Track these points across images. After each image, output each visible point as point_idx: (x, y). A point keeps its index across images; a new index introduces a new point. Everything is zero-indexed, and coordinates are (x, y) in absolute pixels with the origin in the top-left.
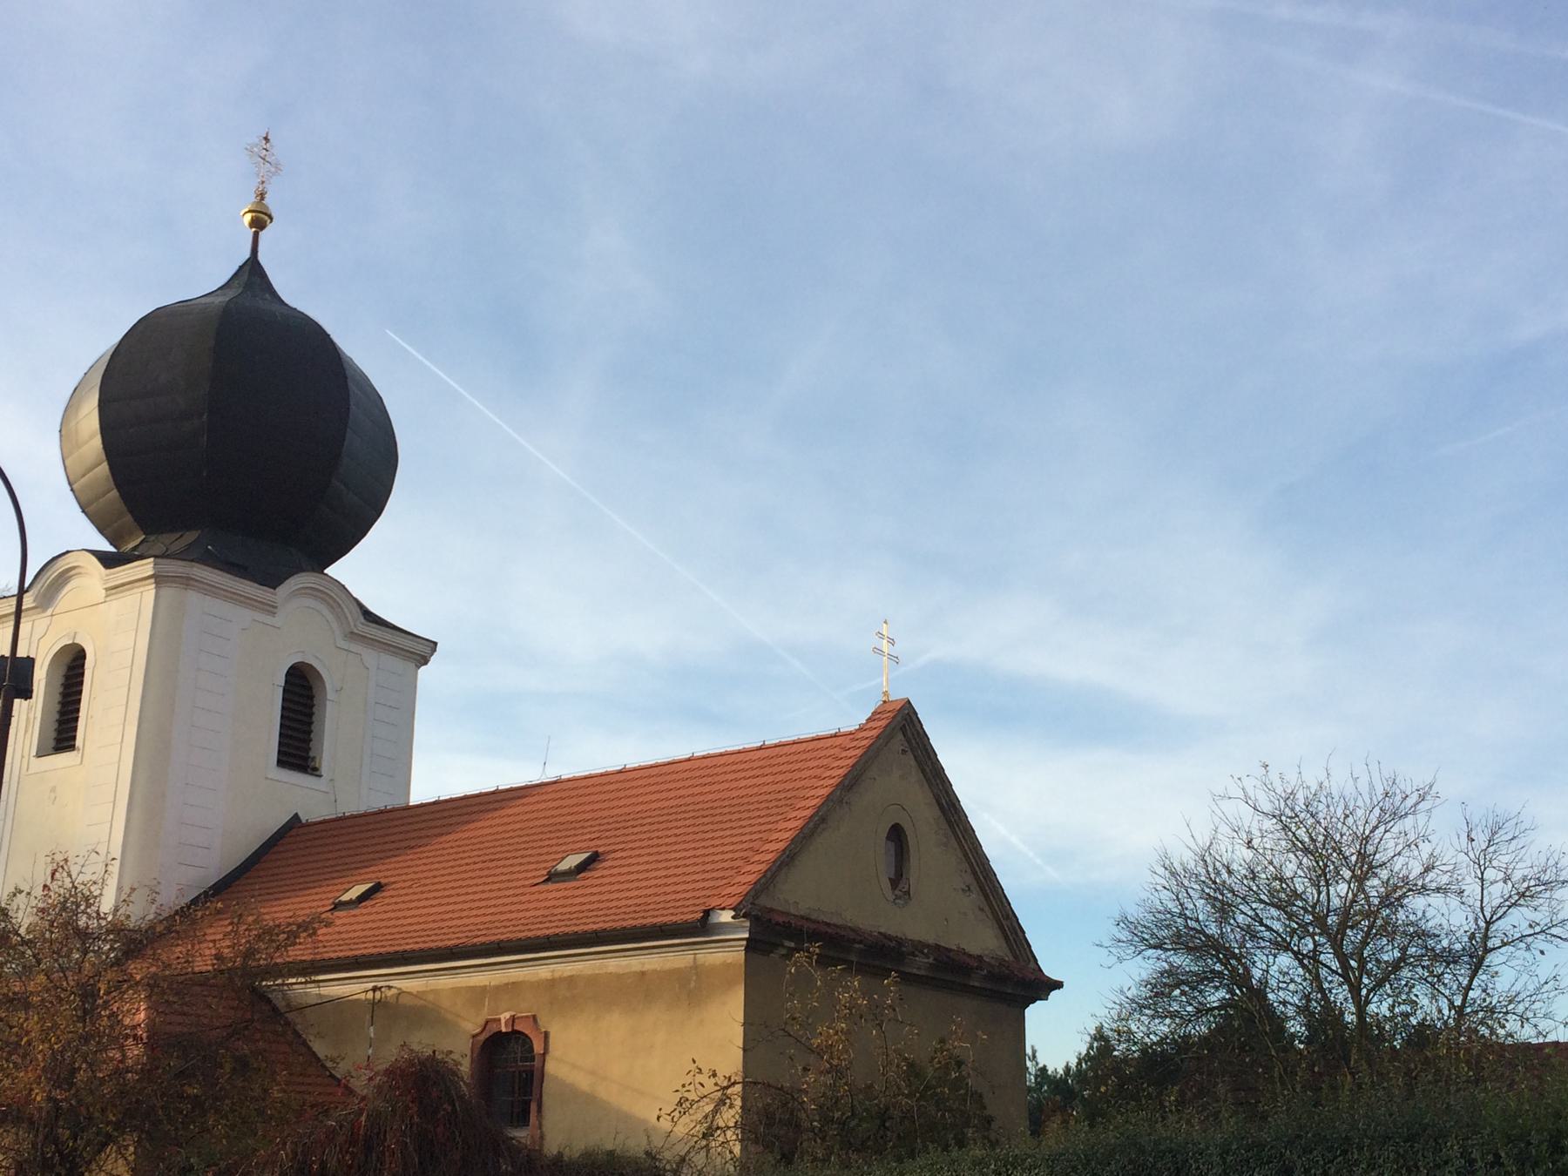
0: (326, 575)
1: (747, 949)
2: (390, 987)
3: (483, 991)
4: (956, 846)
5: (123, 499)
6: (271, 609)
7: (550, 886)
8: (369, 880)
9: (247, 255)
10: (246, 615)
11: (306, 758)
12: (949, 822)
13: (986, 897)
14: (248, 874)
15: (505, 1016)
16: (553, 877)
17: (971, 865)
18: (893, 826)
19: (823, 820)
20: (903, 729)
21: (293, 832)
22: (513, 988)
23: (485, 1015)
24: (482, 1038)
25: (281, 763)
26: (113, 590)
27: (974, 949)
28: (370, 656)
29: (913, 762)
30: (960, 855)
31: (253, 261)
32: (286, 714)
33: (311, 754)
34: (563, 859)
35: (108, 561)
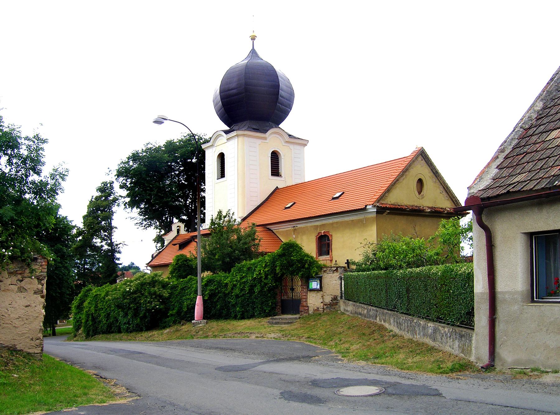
0: (279, 128)
1: (376, 213)
2: (297, 226)
3: (317, 226)
4: (438, 182)
5: (222, 98)
6: (265, 139)
7: (332, 201)
8: (339, 192)
9: (252, 48)
10: (259, 141)
11: (278, 173)
12: (436, 177)
13: (447, 193)
14: (267, 201)
15: (323, 232)
16: (286, 208)
17: (443, 186)
18: (419, 179)
19: (398, 180)
20: (421, 155)
21: (277, 191)
22: (323, 225)
23: (318, 231)
24: (318, 237)
25: (272, 175)
26: (228, 139)
27: (444, 207)
28: (292, 146)
29: (425, 162)
30: (440, 184)
31: (253, 52)
32: (272, 157)
33: (279, 172)
34: (335, 194)
35: (226, 132)
